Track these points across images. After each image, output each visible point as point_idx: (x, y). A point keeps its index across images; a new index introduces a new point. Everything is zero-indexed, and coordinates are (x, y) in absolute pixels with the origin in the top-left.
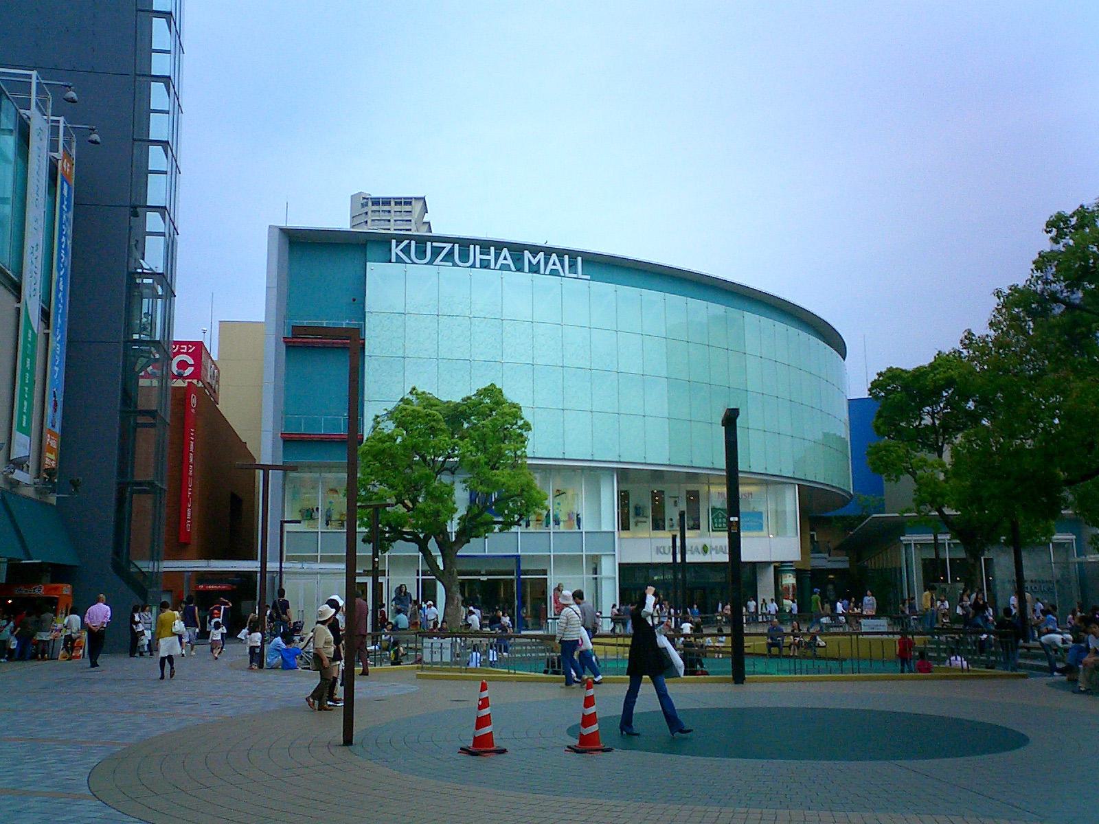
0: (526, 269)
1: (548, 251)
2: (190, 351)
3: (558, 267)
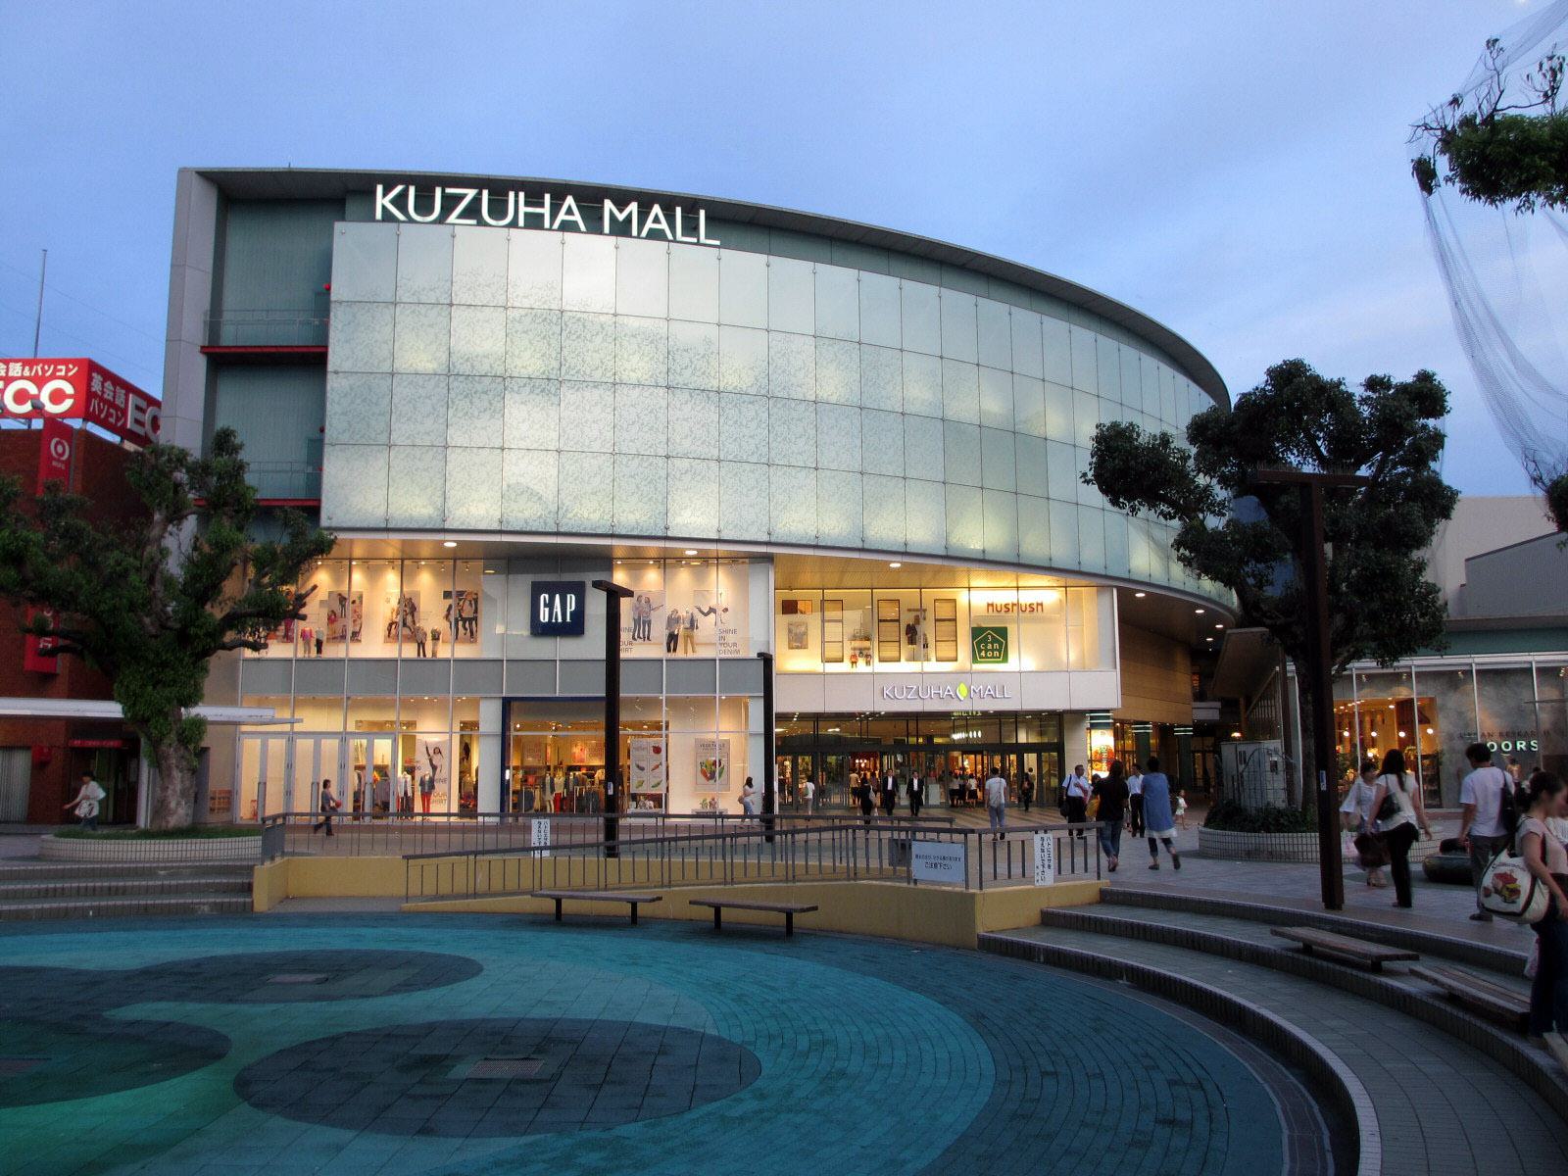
0: (607, 229)
1: (646, 200)
2: (70, 374)
3: (664, 225)
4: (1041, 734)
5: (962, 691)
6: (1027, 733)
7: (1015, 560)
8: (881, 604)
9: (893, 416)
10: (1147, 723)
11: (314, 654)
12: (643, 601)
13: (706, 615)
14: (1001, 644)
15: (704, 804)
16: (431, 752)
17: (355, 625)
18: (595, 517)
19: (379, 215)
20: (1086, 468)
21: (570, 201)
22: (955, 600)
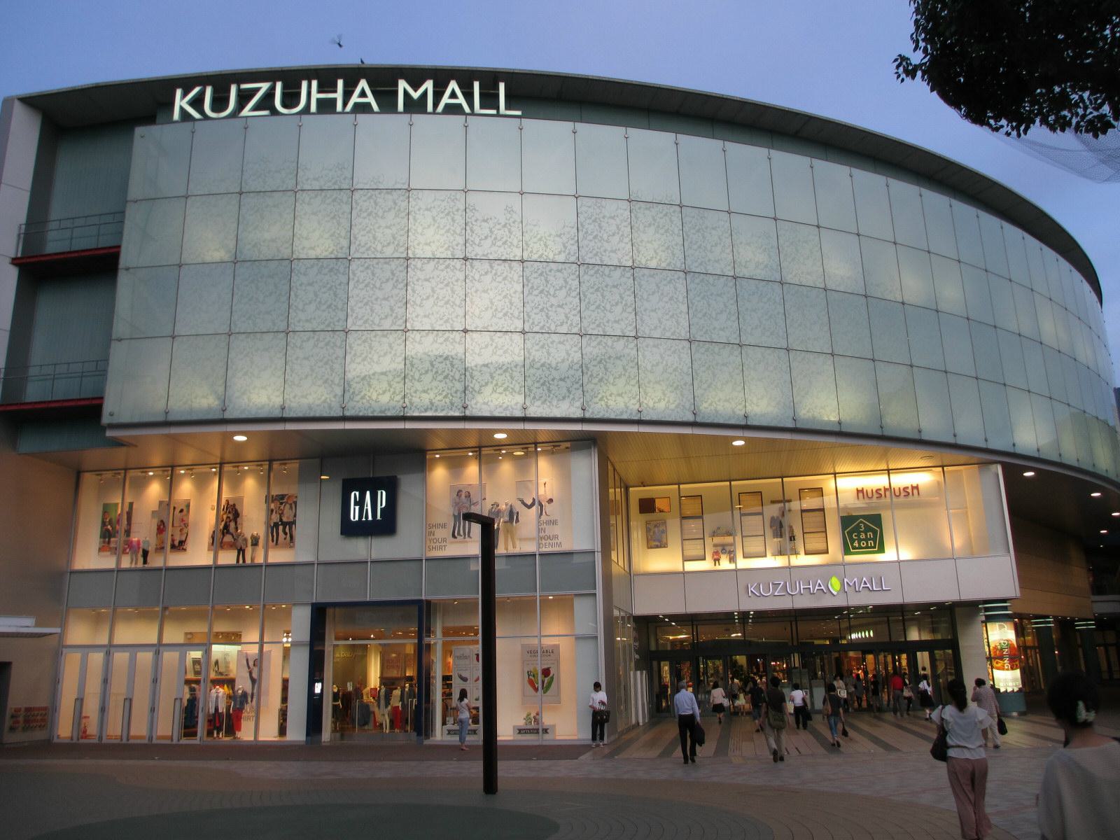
1: (441, 77)
3: (461, 100)
4: (934, 631)
5: (835, 585)
6: (919, 630)
7: (878, 432)
8: (743, 497)
9: (723, 280)
10: (1048, 617)
11: (140, 564)
12: (463, 496)
13: (529, 507)
14: (875, 532)
15: (528, 718)
16: (251, 663)
17: (181, 534)
18: (385, 399)
19: (176, 116)
20: (907, 49)
21: (363, 84)
22: (822, 488)
